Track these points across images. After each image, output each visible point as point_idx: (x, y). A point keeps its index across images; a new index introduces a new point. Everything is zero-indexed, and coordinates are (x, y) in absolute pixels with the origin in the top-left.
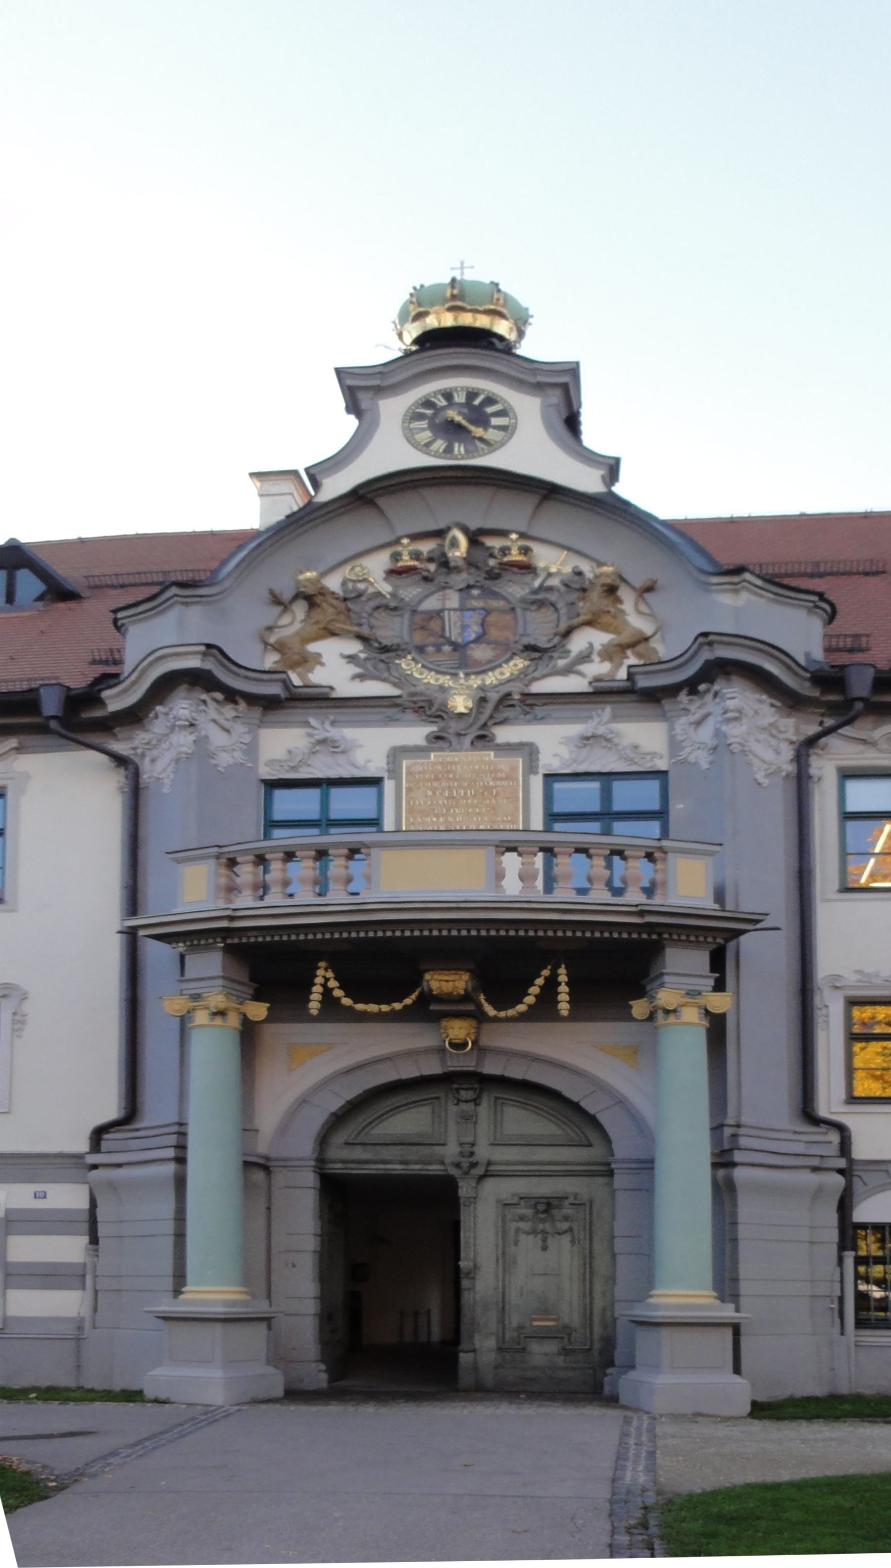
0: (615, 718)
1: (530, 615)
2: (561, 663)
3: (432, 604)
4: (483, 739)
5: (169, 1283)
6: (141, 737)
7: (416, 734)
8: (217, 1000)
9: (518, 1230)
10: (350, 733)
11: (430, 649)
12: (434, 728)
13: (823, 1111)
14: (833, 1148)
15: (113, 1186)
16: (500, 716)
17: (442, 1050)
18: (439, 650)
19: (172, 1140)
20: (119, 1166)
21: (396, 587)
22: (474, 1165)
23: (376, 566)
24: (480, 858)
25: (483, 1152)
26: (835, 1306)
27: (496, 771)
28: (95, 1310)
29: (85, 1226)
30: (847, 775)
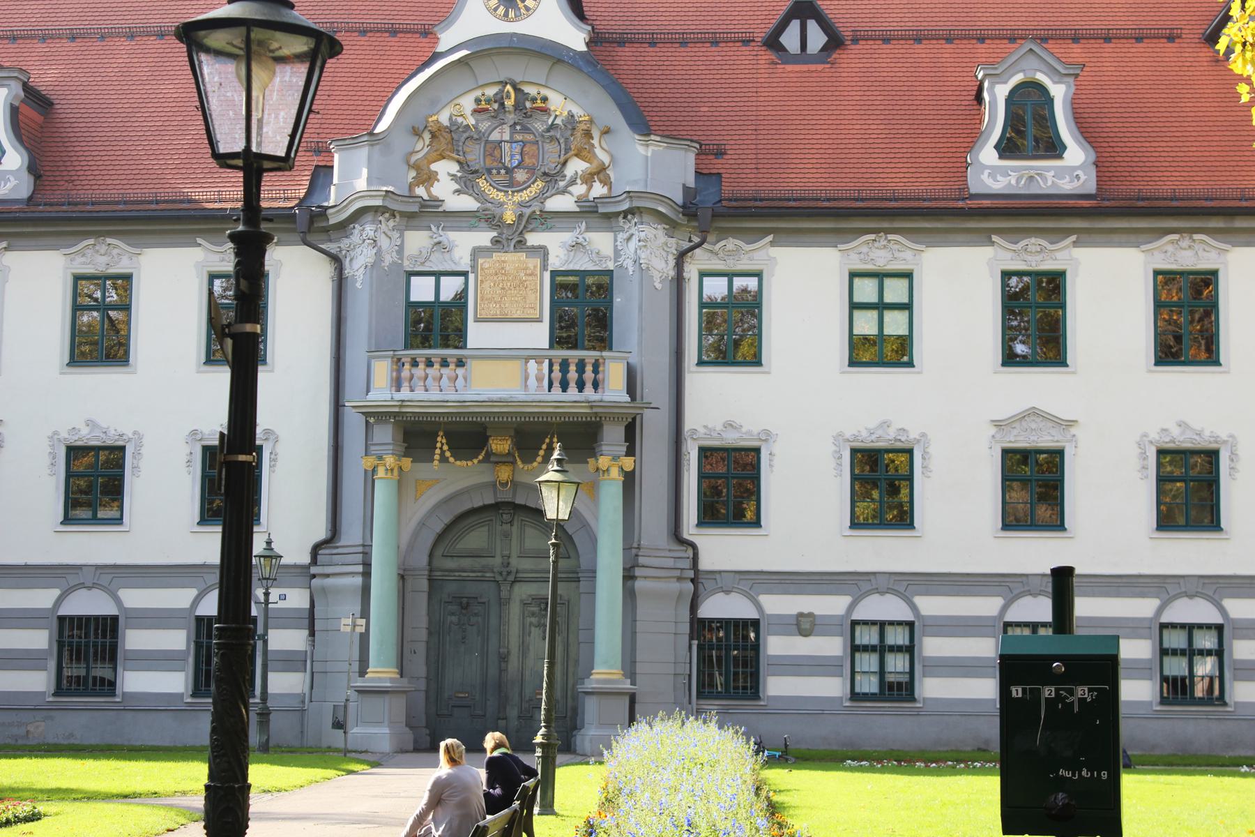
0: (588, 229)
1: (547, 146)
2: (562, 184)
3: (495, 136)
4: (521, 244)
5: (356, 667)
6: (345, 243)
7: (484, 238)
8: (390, 460)
9: (531, 624)
10: (453, 235)
11: (494, 171)
12: (495, 234)
13: (686, 536)
14: (687, 564)
15: (324, 591)
16: (531, 227)
17: (494, 485)
18: (499, 173)
19: (359, 558)
20: (328, 576)
21: (477, 121)
22: (509, 573)
23: (468, 103)
24: (515, 367)
25: (515, 562)
26: (686, 681)
27: (526, 269)
28: (312, 687)
29: (306, 622)
30: (703, 274)
